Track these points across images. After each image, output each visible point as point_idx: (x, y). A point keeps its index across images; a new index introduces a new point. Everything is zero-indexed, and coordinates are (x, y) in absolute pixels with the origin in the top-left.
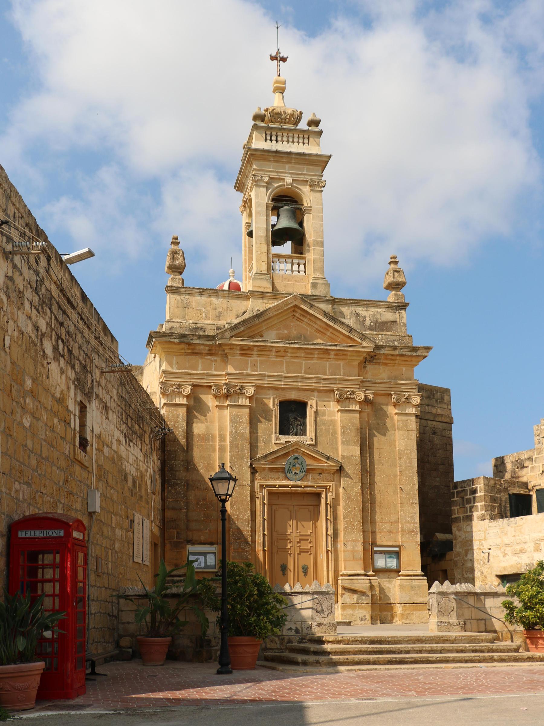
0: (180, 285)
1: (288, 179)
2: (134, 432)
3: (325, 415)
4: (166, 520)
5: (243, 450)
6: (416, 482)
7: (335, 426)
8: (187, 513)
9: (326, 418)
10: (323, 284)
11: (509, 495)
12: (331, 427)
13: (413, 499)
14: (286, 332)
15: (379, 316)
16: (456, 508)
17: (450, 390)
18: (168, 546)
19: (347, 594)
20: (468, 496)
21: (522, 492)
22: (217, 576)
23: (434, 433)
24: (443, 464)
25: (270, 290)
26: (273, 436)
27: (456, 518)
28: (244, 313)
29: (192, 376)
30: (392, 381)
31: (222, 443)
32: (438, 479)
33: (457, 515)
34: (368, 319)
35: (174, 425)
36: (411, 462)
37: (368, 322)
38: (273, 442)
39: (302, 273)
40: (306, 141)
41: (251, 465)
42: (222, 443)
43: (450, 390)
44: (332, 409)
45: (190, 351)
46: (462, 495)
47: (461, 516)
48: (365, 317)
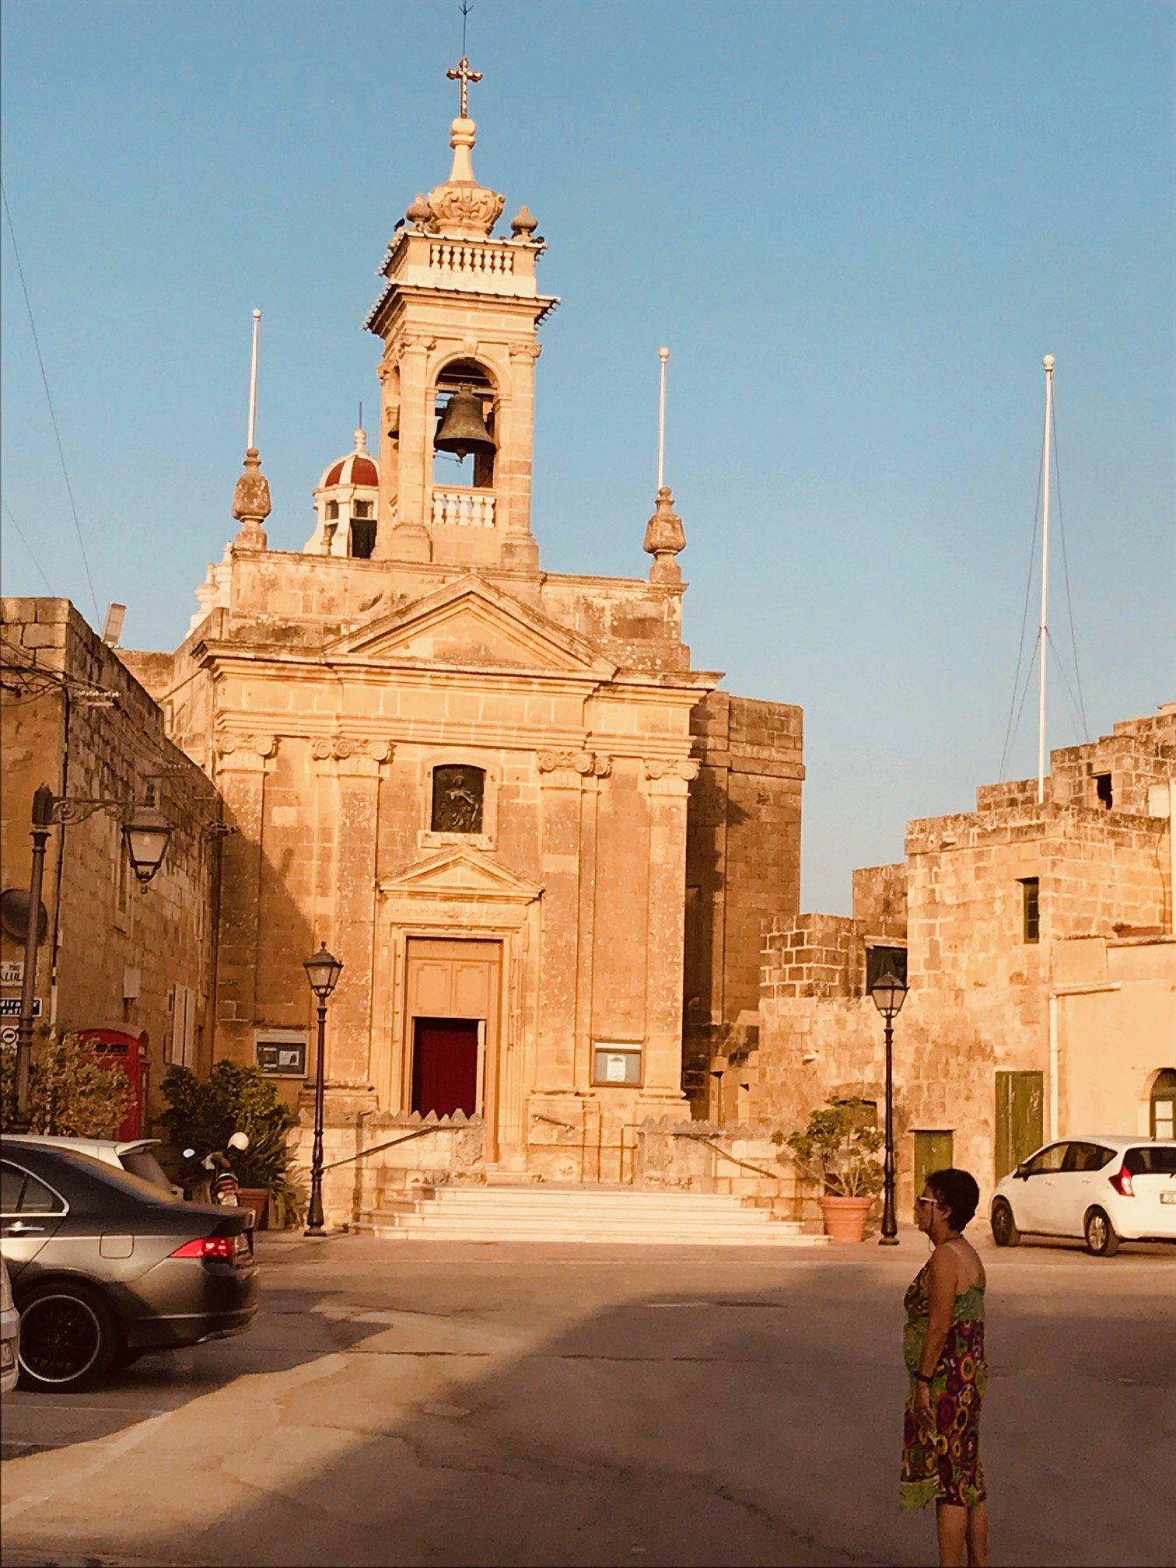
0: (259, 547)
1: (471, 339)
2: (178, 847)
3: (518, 795)
4: (219, 983)
5: (363, 860)
6: (681, 924)
7: (534, 816)
8: (256, 970)
9: (520, 801)
10: (527, 546)
11: (868, 950)
12: (528, 818)
13: (674, 955)
14: (452, 639)
15: (628, 608)
16: (766, 968)
17: (797, 712)
18: (219, 1031)
19: (544, 1127)
20: (788, 949)
21: (893, 945)
22: (307, 1087)
23: (762, 800)
24: (777, 865)
25: (424, 557)
26: (420, 833)
27: (768, 988)
28: (376, 601)
29: (275, 719)
30: (647, 735)
31: (327, 845)
32: (763, 895)
33: (767, 983)
34: (608, 613)
35: (239, 809)
36: (673, 887)
37: (607, 620)
38: (419, 844)
39: (489, 523)
40: (508, 263)
41: (377, 885)
42: (327, 845)
43: (797, 712)
44: (530, 785)
45: (273, 672)
46: (778, 944)
47: (775, 984)
48: (603, 609)
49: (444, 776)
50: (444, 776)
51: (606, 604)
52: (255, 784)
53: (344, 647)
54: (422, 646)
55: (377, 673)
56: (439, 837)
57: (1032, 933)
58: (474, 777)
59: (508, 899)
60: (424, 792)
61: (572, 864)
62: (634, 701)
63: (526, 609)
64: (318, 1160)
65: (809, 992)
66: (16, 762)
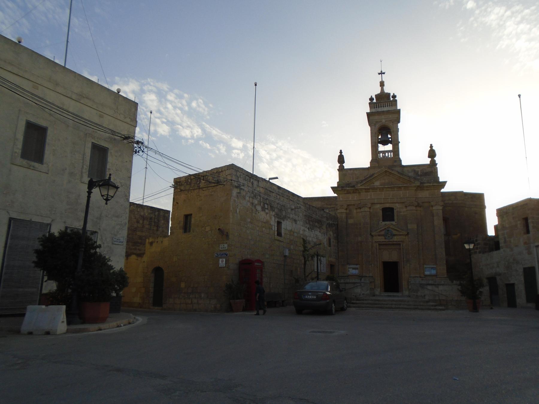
43: (174, 179)
49: (384, 210)
50: (384, 210)
51: (419, 170)
52: (344, 216)
53: (359, 185)
54: (377, 184)
55: (367, 190)
56: (384, 223)
57: (528, 232)
58: (392, 210)
59: (400, 235)
60: (380, 213)
61: (415, 226)
62: (427, 190)
63: (398, 172)
64: (347, 283)
65: (480, 253)
66: (226, 151)
